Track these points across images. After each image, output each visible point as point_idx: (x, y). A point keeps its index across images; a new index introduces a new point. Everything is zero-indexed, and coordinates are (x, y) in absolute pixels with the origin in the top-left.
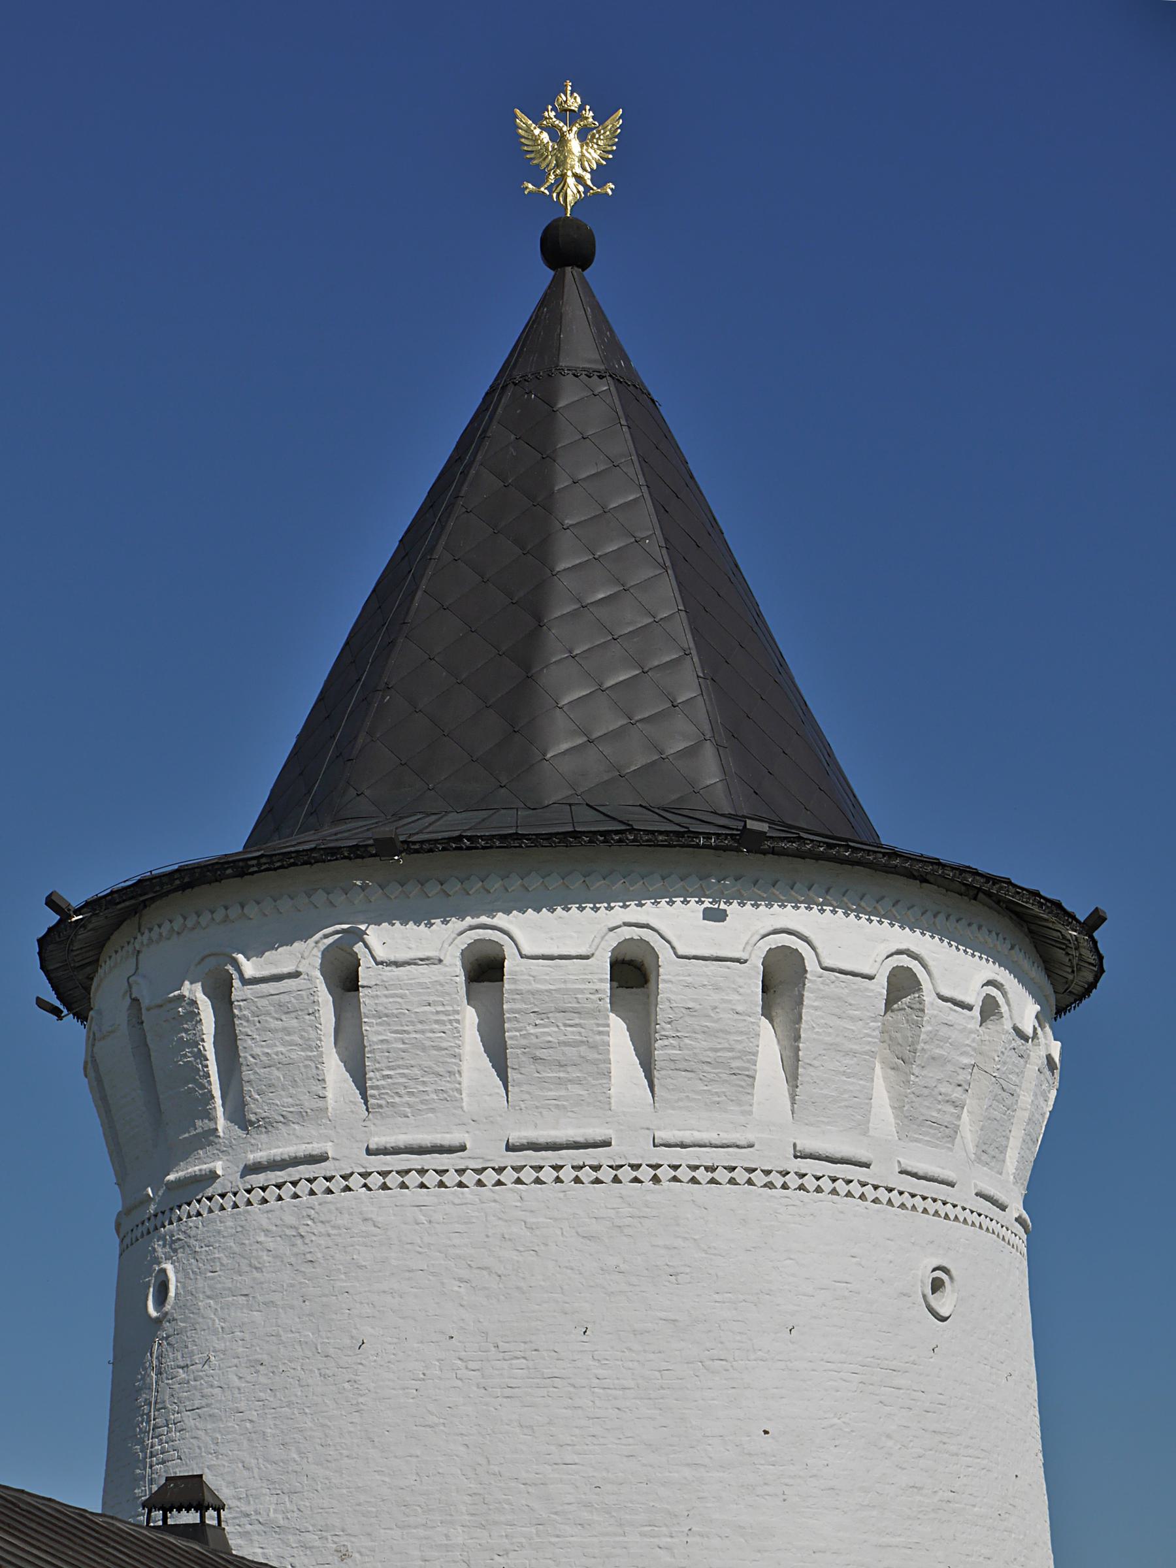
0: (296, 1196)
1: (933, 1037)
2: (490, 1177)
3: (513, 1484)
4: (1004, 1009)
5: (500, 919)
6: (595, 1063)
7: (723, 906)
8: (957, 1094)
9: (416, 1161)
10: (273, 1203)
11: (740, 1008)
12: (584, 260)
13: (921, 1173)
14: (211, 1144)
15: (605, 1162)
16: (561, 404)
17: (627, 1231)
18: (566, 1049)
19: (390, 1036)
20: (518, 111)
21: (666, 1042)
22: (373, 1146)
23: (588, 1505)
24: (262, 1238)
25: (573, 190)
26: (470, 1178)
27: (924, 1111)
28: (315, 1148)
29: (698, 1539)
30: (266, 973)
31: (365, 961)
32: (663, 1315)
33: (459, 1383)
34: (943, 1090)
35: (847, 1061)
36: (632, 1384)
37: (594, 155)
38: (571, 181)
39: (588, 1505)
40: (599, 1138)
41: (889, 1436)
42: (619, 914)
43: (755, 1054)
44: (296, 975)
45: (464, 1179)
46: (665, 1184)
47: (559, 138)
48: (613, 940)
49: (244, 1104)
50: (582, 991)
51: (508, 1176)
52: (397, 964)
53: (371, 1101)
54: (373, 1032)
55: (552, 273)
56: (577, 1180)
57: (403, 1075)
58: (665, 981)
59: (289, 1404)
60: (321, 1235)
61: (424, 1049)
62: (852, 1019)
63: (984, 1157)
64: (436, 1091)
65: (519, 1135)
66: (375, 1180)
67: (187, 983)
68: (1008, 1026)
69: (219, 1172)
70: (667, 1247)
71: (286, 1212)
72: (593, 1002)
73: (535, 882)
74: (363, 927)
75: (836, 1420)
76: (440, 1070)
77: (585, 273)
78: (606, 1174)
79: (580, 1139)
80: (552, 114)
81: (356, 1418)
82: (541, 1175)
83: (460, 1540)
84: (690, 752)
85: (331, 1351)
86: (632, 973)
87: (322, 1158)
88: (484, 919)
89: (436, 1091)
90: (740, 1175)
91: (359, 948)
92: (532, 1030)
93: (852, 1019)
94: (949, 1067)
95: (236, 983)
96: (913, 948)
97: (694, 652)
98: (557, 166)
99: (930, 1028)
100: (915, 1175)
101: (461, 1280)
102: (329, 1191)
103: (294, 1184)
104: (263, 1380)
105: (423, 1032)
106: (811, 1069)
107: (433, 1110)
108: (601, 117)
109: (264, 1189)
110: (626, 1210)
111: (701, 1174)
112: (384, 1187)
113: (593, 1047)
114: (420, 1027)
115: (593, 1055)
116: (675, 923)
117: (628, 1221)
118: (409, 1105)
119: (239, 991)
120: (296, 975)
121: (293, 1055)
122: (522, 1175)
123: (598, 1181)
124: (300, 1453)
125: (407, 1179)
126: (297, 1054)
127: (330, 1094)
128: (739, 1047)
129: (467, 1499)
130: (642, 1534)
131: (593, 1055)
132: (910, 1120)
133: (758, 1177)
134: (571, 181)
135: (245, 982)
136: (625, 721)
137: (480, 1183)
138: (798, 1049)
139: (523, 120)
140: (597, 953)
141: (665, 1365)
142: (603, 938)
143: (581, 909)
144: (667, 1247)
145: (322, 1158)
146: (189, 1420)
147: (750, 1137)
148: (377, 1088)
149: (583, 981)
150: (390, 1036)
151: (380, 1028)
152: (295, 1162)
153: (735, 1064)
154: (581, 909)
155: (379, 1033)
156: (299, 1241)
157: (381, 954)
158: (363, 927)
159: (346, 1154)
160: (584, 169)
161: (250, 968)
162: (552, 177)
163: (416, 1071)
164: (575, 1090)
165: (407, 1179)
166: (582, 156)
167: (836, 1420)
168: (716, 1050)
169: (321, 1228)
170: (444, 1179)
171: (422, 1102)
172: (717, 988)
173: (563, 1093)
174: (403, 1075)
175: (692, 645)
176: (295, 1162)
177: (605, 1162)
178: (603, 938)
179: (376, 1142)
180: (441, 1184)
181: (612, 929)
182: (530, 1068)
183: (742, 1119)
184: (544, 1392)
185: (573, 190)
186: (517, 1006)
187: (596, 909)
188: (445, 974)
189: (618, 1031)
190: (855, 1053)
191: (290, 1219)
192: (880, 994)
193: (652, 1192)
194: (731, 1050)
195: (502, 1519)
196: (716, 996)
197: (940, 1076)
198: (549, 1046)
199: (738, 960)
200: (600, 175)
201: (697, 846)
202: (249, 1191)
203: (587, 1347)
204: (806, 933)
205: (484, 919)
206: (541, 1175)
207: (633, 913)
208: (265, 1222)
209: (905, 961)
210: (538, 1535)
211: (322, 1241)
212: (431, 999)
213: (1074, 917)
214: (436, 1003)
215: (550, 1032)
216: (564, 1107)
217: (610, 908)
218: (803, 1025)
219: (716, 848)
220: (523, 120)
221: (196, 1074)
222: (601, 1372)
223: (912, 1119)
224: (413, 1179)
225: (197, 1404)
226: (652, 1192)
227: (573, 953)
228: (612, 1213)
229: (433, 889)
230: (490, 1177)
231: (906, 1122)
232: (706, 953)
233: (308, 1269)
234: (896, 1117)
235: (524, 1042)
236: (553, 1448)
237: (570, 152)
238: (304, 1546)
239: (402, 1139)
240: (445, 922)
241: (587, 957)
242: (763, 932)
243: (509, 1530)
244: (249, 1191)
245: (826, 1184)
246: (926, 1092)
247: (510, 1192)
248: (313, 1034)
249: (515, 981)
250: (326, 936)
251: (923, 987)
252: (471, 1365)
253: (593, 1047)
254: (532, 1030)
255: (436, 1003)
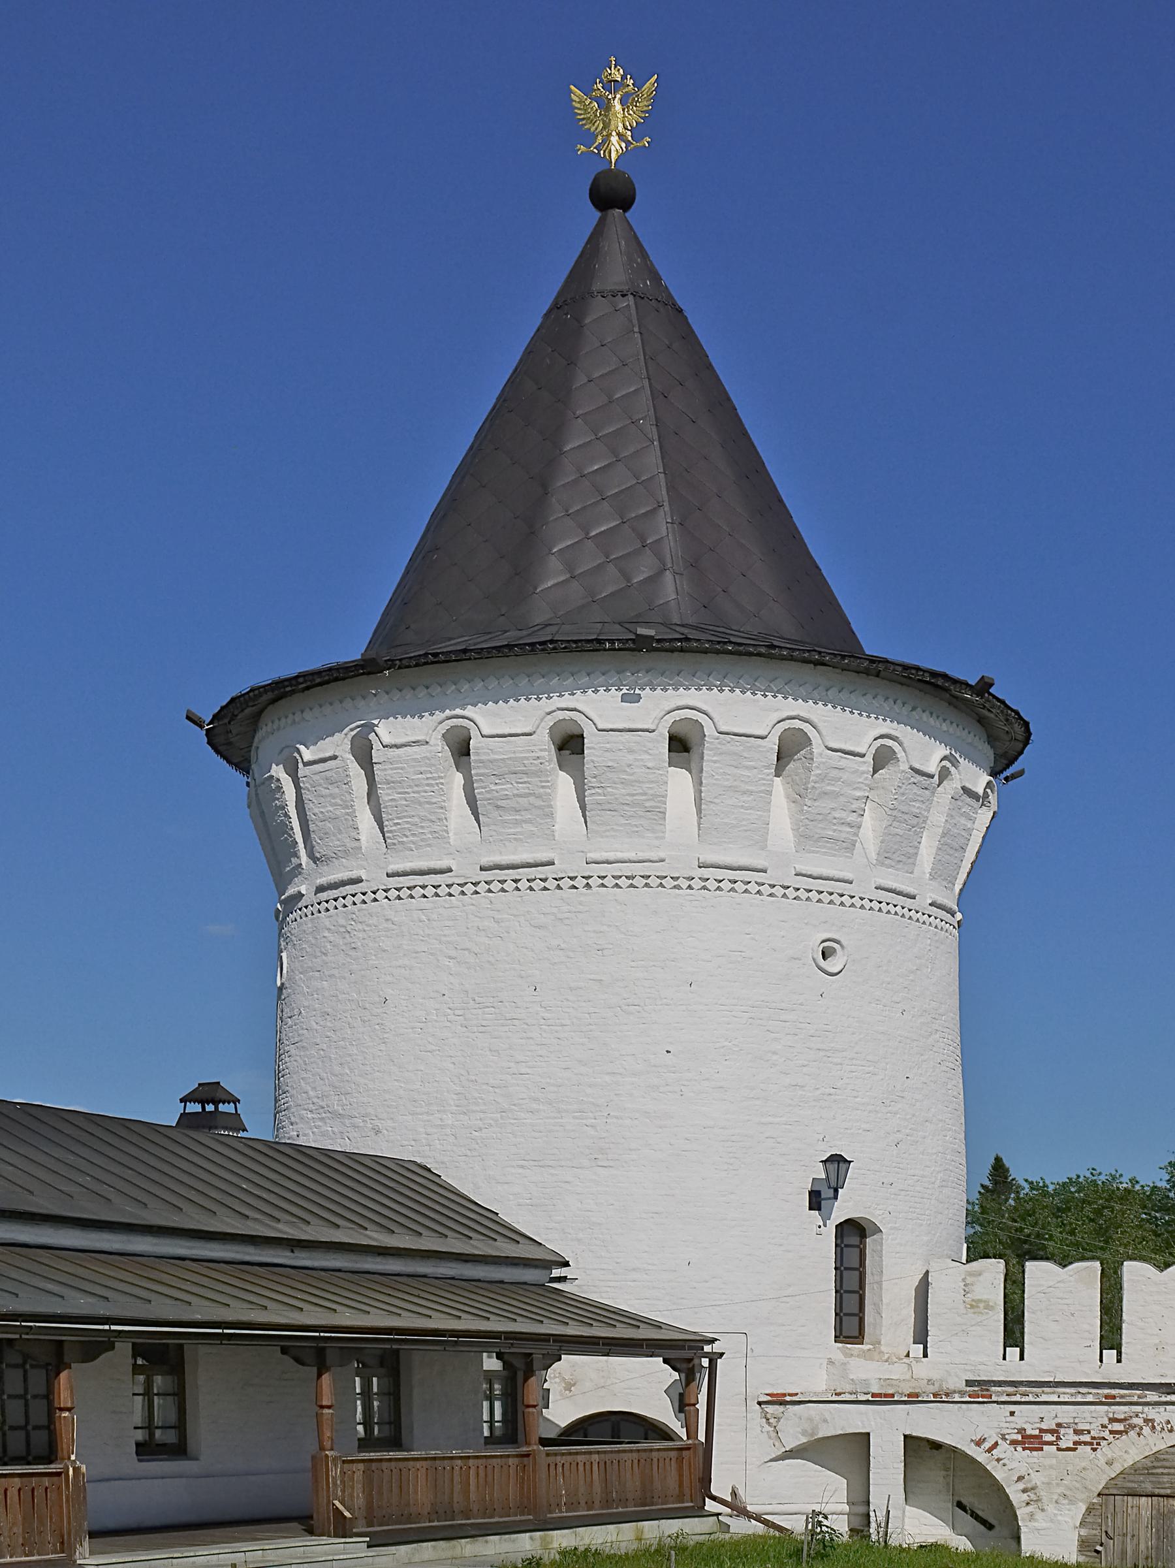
0: (345, 906)
1: (823, 778)
2: (470, 888)
3: (484, 1087)
4: (900, 754)
5: (469, 711)
6: (539, 808)
7: (637, 691)
8: (852, 818)
9: (420, 880)
10: (332, 911)
11: (650, 765)
12: (626, 203)
13: (815, 874)
14: (300, 873)
15: (550, 876)
16: (587, 321)
17: (567, 922)
18: (520, 800)
19: (396, 796)
20: (572, 87)
21: (593, 791)
22: (390, 871)
23: (536, 1100)
24: (326, 934)
25: (616, 147)
26: (455, 890)
27: (819, 831)
28: (354, 874)
29: (615, 1120)
30: (316, 757)
31: (376, 745)
32: (592, 977)
33: (449, 1024)
34: (837, 816)
35: (745, 798)
36: (568, 1022)
37: (633, 118)
38: (614, 139)
39: (536, 1100)
40: (759, 867)
41: (775, 1053)
42: (557, 702)
43: (665, 796)
44: (335, 757)
45: (452, 891)
46: (595, 889)
47: (606, 106)
48: (550, 721)
49: (313, 847)
50: (527, 758)
51: (482, 887)
52: (396, 746)
53: (388, 841)
54: (383, 793)
55: (598, 214)
56: (531, 889)
57: (408, 823)
58: (589, 748)
59: (343, 1039)
60: (359, 931)
61: (420, 804)
62: (747, 768)
63: (887, 862)
64: (431, 832)
65: (486, 860)
66: (393, 894)
67: (274, 766)
68: (904, 766)
69: (303, 892)
70: (594, 931)
71: (339, 917)
72: (536, 765)
73: (493, 683)
74: (376, 722)
75: (726, 1043)
76: (433, 818)
77: (627, 214)
78: (551, 884)
79: (531, 861)
80: (600, 86)
81: (383, 1047)
82: (505, 886)
83: (450, 1122)
84: (654, 580)
85: (367, 1006)
86: (790, 749)
87: (359, 881)
88: (458, 711)
89: (431, 832)
90: (654, 882)
91: (372, 736)
92: (493, 787)
93: (747, 768)
94: (842, 799)
95: (300, 765)
96: (802, 714)
97: (666, 504)
98: (604, 128)
99: (819, 772)
100: (810, 876)
101: (450, 958)
102: (364, 902)
103: (344, 898)
104: (329, 1024)
105: (418, 792)
106: (712, 805)
107: (429, 845)
108: (638, 85)
109: (327, 902)
110: (565, 908)
111: (623, 882)
112: (399, 898)
113: (539, 797)
114: (416, 789)
115: (539, 803)
116: (598, 706)
117: (567, 915)
118: (414, 843)
119: (302, 771)
120: (335, 757)
121: (338, 813)
122: (492, 887)
123: (545, 889)
124: (350, 1069)
125: (413, 893)
126: (340, 812)
127: (363, 838)
128: (651, 792)
129: (455, 1097)
130: (574, 1118)
131: (539, 803)
132: (805, 838)
133: (668, 882)
134: (614, 139)
135: (306, 764)
136: (603, 559)
137: (463, 893)
138: (701, 792)
139: (576, 93)
140: (538, 731)
141: (592, 1010)
142: (542, 720)
143: (528, 699)
144: (594, 931)
145: (359, 881)
146: (293, 1050)
147: (662, 855)
148: (390, 832)
149: (528, 751)
150: (396, 796)
151: (389, 791)
152: (343, 883)
153: (647, 804)
154: (528, 699)
155: (389, 795)
156: (347, 936)
157: (387, 739)
158: (376, 722)
159: (374, 877)
160: (626, 129)
161: (307, 754)
162: (600, 138)
163: (416, 819)
164: (528, 827)
165: (413, 893)
166: (621, 117)
167: (726, 1043)
168: (634, 795)
169: (360, 927)
170: (438, 891)
171: (422, 840)
172: (631, 751)
173: (519, 830)
174: (408, 823)
175: (666, 498)
176: (343, 883)
177: (550, 876)
178: (542, 720)
179: (392, 868)
180: (437, 895)
181: (549, 713)
182: (495, 814)
183: (657, 843)
184: (506, 1028)
185: (616, 147)
186: (482, 771)
187: (539, 699)
188: (431, 752)
189: (564, 782)
190: (751, 793)
191: (342, 922)
192: (772, 749)
193: (586, 895)
194: (645, 794)
195: (477, 1108)
196: (630, 758)
197: (833, 805)
198: (506, 797)
199: (647, 730)
200: (637, 131)
201: (605, 650)
202: (319, 904)
203: (538, 999)
204: (704, 707)
205: (458, 711)
206: (505, 886)
207: (567, 701)
208: (327, 923)
209: (797, 724)
210: (502, 1117)
211: (360, 935)
212: (422, 769)
213: (967, 685)
214: (426, 772)
215: (507, 788)
216: (521, 840)
217: (549, 698)
218: (704, 774)
219: (620, 649)
220: (576, 93)
221: (286, 828)
222: (547, 1015)
223: (807, 837)
224: (418, 891)
225: (296, 1039)
226: (586, 895)
227: (519, 731)
228: (555, 910)
229: (422, 693)
230: (470, 888)
231: (802, 839)
232: (620, 726)
233: (352, 953)
234: (795, 836)
235: (488, 796)
236: (512, 1064)
237: (615, 114)
238: (354, 1126)
239: (424, 864)
240: (432, 714)
241: (530, 734)
242: (667, 709)
243: (482, 1115)
244: (319, 904)
245: (753, 888)
246: (820, 817)
247: (483, 899)
248: (348, 797)
249: (477, 754)
250: (352, 730)
251: (813, 742)
252: (457, 1012)
253: (539, 797)
254: (493, 787)
255: (426, 772)
